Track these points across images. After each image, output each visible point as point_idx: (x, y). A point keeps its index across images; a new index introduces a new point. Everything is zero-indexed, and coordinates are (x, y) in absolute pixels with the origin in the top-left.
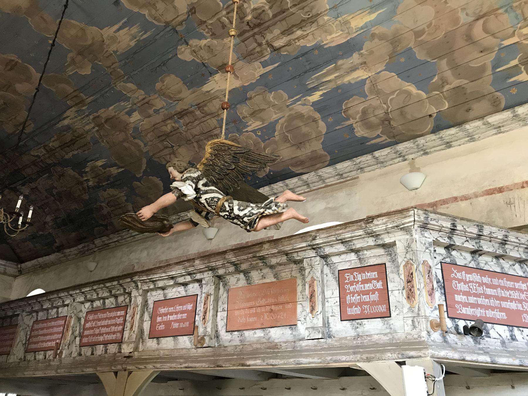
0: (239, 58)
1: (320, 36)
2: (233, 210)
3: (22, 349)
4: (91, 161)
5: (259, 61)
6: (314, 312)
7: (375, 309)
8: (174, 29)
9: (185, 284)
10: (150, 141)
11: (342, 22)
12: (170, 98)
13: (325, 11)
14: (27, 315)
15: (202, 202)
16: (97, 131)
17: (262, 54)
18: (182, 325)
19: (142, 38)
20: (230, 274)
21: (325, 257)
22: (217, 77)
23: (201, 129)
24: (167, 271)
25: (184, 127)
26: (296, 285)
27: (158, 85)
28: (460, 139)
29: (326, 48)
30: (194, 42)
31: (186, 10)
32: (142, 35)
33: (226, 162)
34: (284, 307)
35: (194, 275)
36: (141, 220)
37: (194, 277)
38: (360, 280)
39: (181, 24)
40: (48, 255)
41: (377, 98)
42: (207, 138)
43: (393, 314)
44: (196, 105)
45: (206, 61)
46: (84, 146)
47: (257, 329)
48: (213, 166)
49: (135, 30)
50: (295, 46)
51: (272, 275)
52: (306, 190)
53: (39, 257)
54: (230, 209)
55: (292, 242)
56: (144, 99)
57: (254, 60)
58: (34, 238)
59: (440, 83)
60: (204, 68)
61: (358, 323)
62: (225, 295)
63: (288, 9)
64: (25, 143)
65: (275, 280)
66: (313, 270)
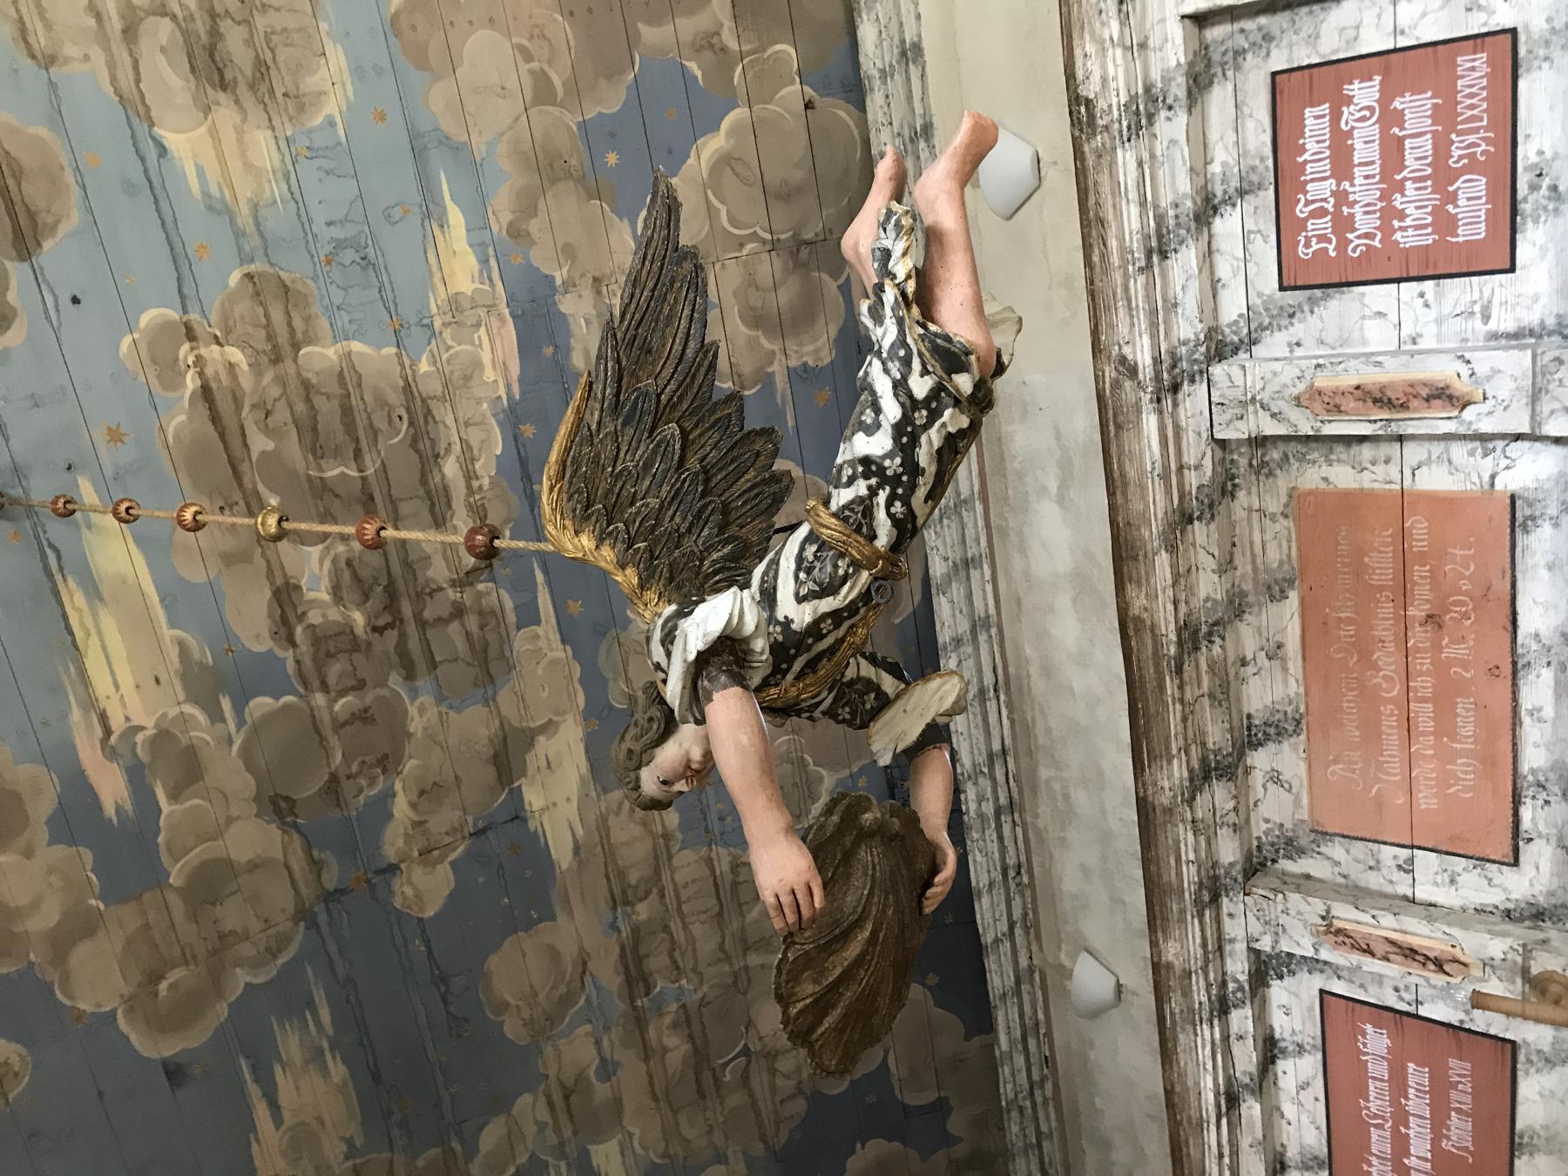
0: (487, 701)
1: (479, 403)
2: (866, 461)
5: (513, 632)
6: (1462, 387)
7: (1472, 107)
8: (331, 897)
9: (1270, 1050)
10: (710, 1133)
11: (449, 317)
12: (567, 1000)
13: (403, 366)
15: (808, 619)
17: (493, 613)
18: (1462, 1097)
19: (329, 1029)
20: (1243, 807)
21: (1219, 348)
22: (533, 798)
23: (704, 917)
24: (1194, 1113)
25: (684, 982)
26: (1324, 493)
27: (513, 1029)
28: (898, 14)
29: (522, 394)
30: (393, 842)
31: (274, 831)
32: (318, 1023)
33: (648, 465)
34: (1422, 558)
35: (1231, 986)
36: (813, 920)
37: (1241, 989)
38: (1331, 184)
39: (316, 866)
41: (718, 266)
42: (740, 905)
43: (1503, 18)
44: (614, 908)
45: (470, 820)
47: (1515, 699)
48: (657, 541)
49: (291, 1044)
50: (489, 495)
51: (1274, 608)
52: (988, 575)
54: (866, 476)
55: (1132, 473)
56: (551, 1105)
57: (506, 647)
59: (708, 55)
60: (490, 834)
61: (1534, 188)
62: (1336, 850)
63: (364, 479)
65: (1294, 596)
66: (1264, 397)
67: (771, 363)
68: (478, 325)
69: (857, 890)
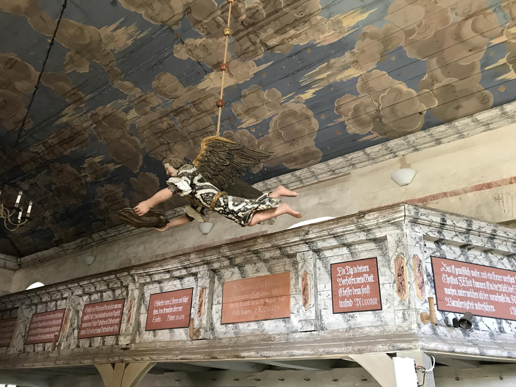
0: (233, 57)
1: (313, 36)
2: (227, 205)
3: (22, 341)
4: (89, 157)
5: (254, 59)
6: (307, 305)
7: (366, 302)
8: (170, 28)
9: (181, 278)
10: (147, 138)
11: (335, 21)
12: (167, 96)
13: (317, 11)
14: (27, 308)
15: (198, 197)
16: (95, 128)
17: (257, 53)
18: (178, 318)
19: (138, 37)
20: (225, 267)
21: (317, 251)
22: (212, 75)
23: (197, 126)
24: (163, 265)
25: (180, 124)
26: (289, 278)
27: (155, 83)
28: (450, 136)
29: (319, 47)
30: (189, 41)
31: (181, 10)
32: (139, 35)
33: (221, 158)
34: (277, 300)
35: (190, 269)
38: (352, 273)
39: (177, 23)
40: (47, 249)
41: (369, 96)
42: (202, 135)
43: (384, 307)
44: (192, 103)
45: (202, 60)
46: (82, 142)
47: (251, 321)
48: (208, 162)
49: (132, 29)
50: (288, 45)
51: (266, 269)
52: (299, 186)
53: (38, 251)
54: (225, 205)
55: (286, 236)
56: (140, 97)
57: (248, 59)
58: (33, 233)
59: (430, 81)
60: (200, 66)
61: (350, 316)
62: (220, 288)
63: (282, 9)
64: (24, 140)
65: (268, 274)
66: (306, 263)
67: (345, 116)
68: (334, 30)
69: (148, 219)
